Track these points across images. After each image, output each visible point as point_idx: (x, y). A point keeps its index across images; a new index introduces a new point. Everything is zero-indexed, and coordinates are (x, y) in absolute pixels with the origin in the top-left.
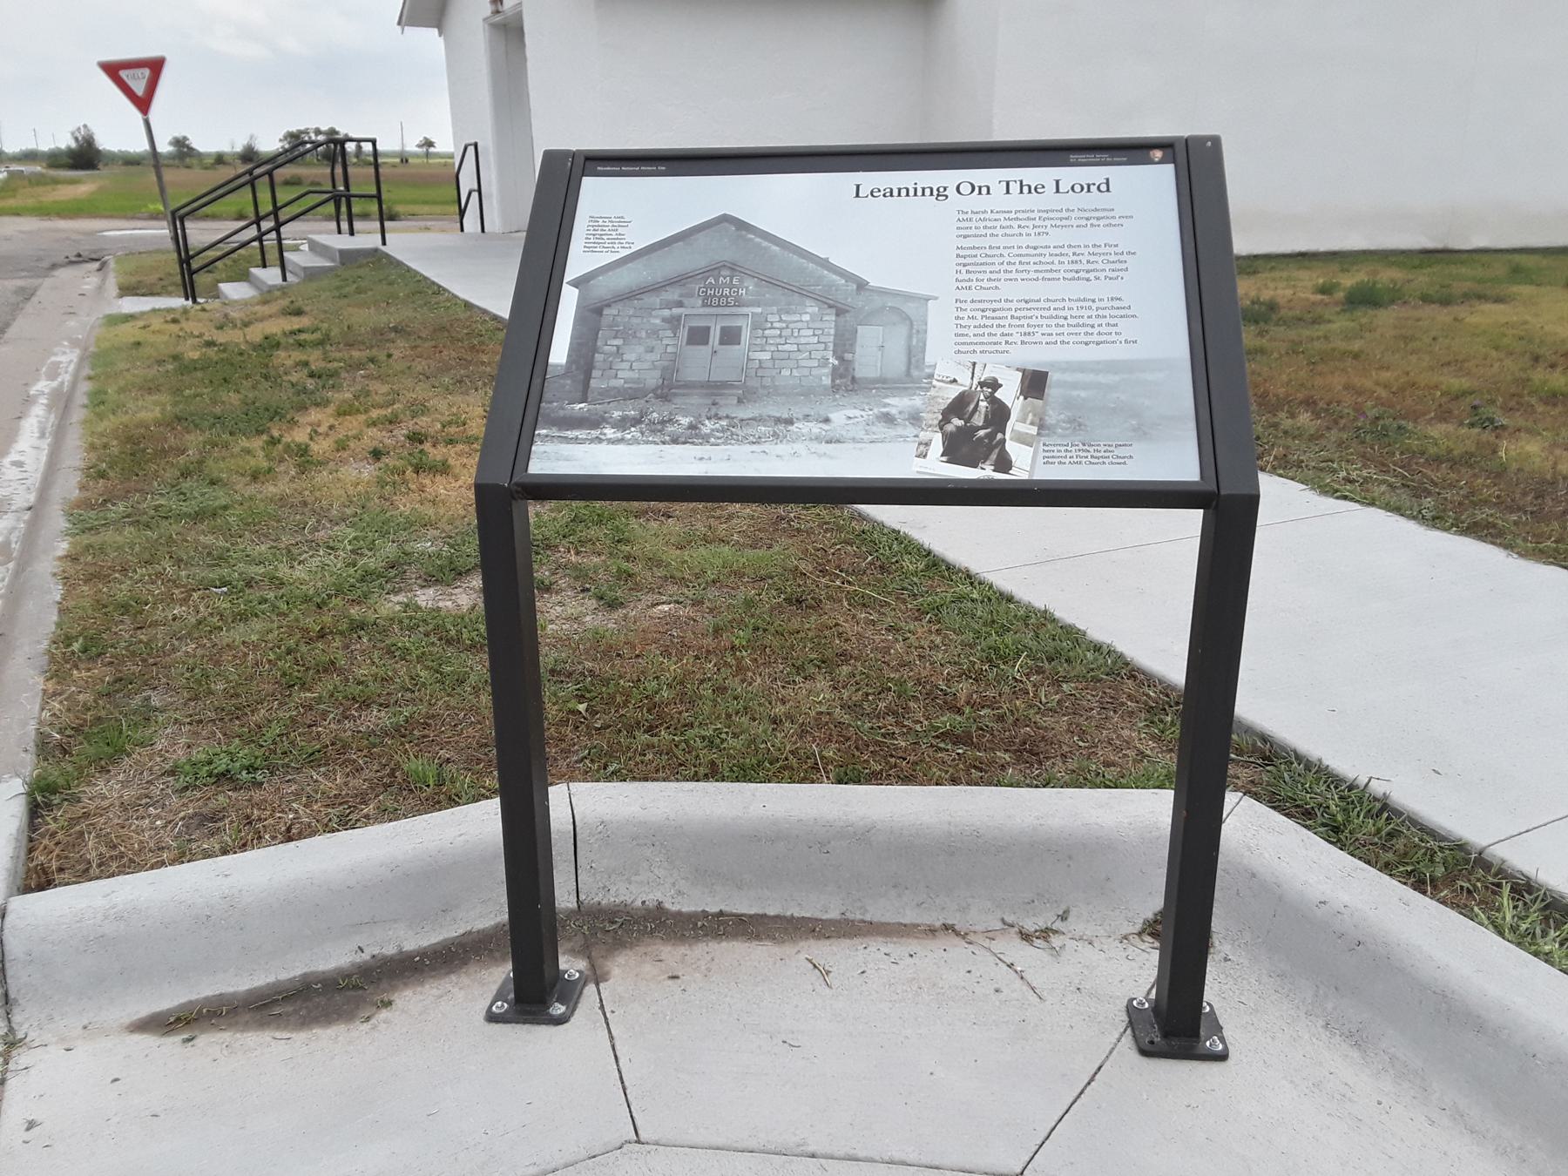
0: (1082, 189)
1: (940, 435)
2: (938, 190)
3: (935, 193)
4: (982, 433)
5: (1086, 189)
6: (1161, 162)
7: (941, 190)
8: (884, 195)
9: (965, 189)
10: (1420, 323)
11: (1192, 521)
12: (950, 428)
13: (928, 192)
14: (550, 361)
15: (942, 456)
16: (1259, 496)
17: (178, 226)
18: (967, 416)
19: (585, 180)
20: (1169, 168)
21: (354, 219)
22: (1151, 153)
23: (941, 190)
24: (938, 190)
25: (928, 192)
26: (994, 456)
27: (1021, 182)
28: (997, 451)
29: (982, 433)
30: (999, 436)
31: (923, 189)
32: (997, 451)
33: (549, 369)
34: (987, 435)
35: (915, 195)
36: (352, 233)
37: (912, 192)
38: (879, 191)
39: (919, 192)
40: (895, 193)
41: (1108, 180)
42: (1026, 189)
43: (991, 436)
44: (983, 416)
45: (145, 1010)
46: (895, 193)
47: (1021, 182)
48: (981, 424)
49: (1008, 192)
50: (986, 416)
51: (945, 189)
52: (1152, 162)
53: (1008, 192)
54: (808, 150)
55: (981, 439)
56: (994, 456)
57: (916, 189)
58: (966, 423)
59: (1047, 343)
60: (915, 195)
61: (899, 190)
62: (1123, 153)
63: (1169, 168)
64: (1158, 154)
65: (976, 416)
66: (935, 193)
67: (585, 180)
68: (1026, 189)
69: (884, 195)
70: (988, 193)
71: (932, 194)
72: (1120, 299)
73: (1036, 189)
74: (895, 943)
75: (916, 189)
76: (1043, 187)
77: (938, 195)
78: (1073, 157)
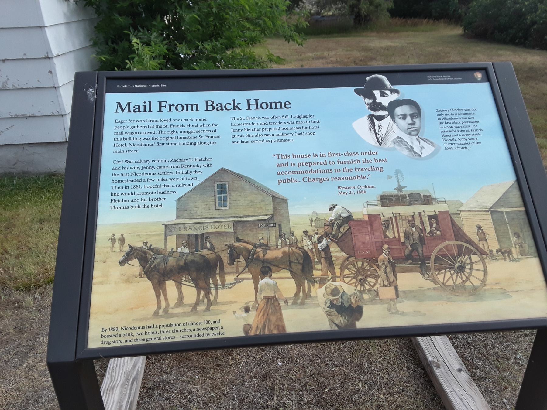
2: (214, 108)
3: (380, 169)
5: (326, 172)
6: (482, 81)
8: (338, 180)
9: (305, 180)
10: (26, 151)
11: (255, 105)
13: (137, 139)
22: (475, 74)
24: (380, 168)
25: (137, 139)
27: (282, 155)
35: (145, 111)
36: (405, 216)
37: (142, 109)
41: (326, 161)
42: (283, 157)
46: (280, 165)
47: (282, 155)
49: (278, 158)
51: (382, 168)
52: (475, 81)
53: (278, 158)
60: (145, 111)
64: (479, 75)
68: (283, 157)
69: (338, 180)
70: (197, 110)
71: (379, 170)
72: (205, 120)
73: (370, 161)
75: (145, 106)
76: (290, 104)
78: (430, 77)
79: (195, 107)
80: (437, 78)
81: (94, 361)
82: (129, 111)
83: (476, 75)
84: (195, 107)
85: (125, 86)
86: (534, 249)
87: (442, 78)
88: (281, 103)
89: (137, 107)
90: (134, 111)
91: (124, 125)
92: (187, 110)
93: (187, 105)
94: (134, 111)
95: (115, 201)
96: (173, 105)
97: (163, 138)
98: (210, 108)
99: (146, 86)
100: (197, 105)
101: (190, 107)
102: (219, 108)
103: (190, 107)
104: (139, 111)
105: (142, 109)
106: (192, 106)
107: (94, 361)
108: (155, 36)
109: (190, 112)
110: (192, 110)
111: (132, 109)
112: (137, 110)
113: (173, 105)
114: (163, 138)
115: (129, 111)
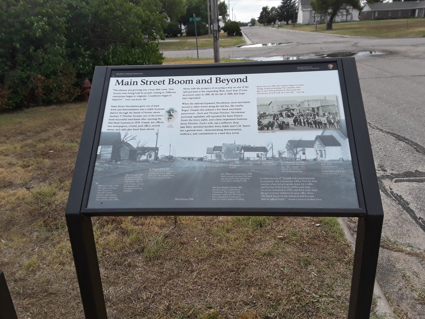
0: (235, 81)
2: (220, 82)
5: (236, 81)
6: (333, 69)
14: (102, 131)
16: (383, 215)
19: (111, 78)
20: (336, 72)
22: (328, 65)
31: (134, 82)
33: (101, 135)
35: (131, 85)
37: (129, 84)
38: (157, 82)
39: (132, 84)
40: (201, 82)
46: (201, 82)
52: (328, 69)
54: (190, 66)
57: (131, 82)
59: (193, 134)
60: (131, 85)
61: (202, 80)
62: (142, 71)
63: (336, 72)
64: (331, 66)
67: (111, 78)
70: (192, 83)
75: (131, 82)
79: (191, 82)
80: (303, 68)
81: (93, 219)
82: (122, 84)
83: (330, 66)
84: (191, 82)
85: (121, 74)
86: (94, 174)
87: (307, 68)
88: (205, 80)
89: (198, 81)
90: (125, 85)
91: (293, 87)
92: (186, 83)
93: (186, 81)
94: (125, 85)
95: (191, 124)
96: (152, 81)
97: (138, 96)
98: (218, 81)
99: (132, 74)
100: (192, 81)
101: (188, 82)
102: (126, 84)
103: (188, 82)
104: (199, 83)
105: (129, 84)
106: (189, 81)
107: (93, 219)
108: (45, 54)
109: (188, 84)
110: (189, 83)
111: (124, 83)
112: (198, 82)
113: (152, 81)
114: (138, 96)
115: (122, 84)
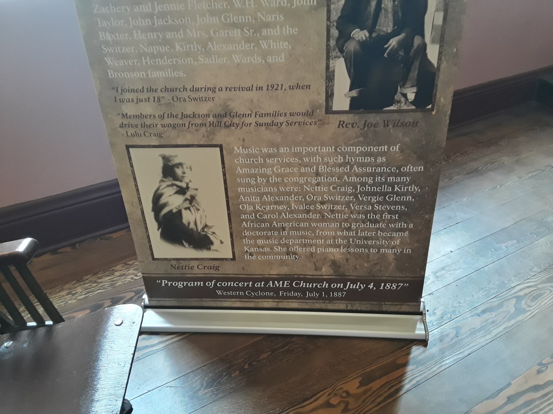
1: (342, 60)
2: (216, 267)
4: (393, 42)
7: (217, 267)
12: (351, 46)
15: (351, 89)
17: (20, 281)
18: (370, 22)
21: (47, 292)
23: (217, 267)
24: (216, 267)
26: (414, 74)
28: (417, 64)
29: (393, 42)
30: (417, 41)
32: (417, 64)
34: (400, 43)
43: (406, 45)
44: (390, 16)
45: (197, 218)
48: (390, 30)
50: (395, 14)
55: (394, 52)
56: (414, 74)
58: (370, 33)
65: (382, 18)
66: (172, 126)
71: (214, 269)
74: (437, 81)
77: (216, 269)
